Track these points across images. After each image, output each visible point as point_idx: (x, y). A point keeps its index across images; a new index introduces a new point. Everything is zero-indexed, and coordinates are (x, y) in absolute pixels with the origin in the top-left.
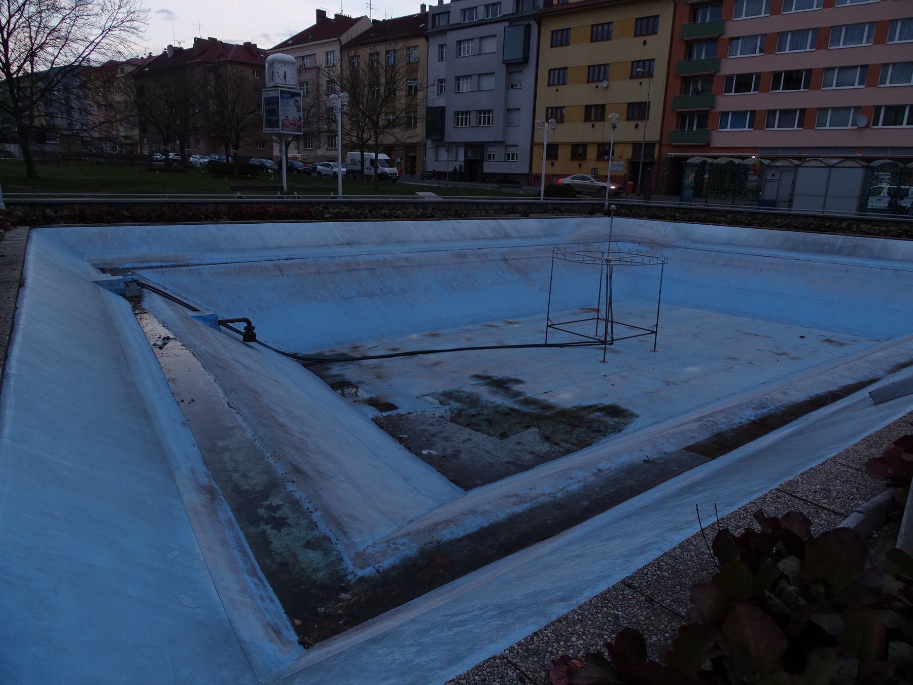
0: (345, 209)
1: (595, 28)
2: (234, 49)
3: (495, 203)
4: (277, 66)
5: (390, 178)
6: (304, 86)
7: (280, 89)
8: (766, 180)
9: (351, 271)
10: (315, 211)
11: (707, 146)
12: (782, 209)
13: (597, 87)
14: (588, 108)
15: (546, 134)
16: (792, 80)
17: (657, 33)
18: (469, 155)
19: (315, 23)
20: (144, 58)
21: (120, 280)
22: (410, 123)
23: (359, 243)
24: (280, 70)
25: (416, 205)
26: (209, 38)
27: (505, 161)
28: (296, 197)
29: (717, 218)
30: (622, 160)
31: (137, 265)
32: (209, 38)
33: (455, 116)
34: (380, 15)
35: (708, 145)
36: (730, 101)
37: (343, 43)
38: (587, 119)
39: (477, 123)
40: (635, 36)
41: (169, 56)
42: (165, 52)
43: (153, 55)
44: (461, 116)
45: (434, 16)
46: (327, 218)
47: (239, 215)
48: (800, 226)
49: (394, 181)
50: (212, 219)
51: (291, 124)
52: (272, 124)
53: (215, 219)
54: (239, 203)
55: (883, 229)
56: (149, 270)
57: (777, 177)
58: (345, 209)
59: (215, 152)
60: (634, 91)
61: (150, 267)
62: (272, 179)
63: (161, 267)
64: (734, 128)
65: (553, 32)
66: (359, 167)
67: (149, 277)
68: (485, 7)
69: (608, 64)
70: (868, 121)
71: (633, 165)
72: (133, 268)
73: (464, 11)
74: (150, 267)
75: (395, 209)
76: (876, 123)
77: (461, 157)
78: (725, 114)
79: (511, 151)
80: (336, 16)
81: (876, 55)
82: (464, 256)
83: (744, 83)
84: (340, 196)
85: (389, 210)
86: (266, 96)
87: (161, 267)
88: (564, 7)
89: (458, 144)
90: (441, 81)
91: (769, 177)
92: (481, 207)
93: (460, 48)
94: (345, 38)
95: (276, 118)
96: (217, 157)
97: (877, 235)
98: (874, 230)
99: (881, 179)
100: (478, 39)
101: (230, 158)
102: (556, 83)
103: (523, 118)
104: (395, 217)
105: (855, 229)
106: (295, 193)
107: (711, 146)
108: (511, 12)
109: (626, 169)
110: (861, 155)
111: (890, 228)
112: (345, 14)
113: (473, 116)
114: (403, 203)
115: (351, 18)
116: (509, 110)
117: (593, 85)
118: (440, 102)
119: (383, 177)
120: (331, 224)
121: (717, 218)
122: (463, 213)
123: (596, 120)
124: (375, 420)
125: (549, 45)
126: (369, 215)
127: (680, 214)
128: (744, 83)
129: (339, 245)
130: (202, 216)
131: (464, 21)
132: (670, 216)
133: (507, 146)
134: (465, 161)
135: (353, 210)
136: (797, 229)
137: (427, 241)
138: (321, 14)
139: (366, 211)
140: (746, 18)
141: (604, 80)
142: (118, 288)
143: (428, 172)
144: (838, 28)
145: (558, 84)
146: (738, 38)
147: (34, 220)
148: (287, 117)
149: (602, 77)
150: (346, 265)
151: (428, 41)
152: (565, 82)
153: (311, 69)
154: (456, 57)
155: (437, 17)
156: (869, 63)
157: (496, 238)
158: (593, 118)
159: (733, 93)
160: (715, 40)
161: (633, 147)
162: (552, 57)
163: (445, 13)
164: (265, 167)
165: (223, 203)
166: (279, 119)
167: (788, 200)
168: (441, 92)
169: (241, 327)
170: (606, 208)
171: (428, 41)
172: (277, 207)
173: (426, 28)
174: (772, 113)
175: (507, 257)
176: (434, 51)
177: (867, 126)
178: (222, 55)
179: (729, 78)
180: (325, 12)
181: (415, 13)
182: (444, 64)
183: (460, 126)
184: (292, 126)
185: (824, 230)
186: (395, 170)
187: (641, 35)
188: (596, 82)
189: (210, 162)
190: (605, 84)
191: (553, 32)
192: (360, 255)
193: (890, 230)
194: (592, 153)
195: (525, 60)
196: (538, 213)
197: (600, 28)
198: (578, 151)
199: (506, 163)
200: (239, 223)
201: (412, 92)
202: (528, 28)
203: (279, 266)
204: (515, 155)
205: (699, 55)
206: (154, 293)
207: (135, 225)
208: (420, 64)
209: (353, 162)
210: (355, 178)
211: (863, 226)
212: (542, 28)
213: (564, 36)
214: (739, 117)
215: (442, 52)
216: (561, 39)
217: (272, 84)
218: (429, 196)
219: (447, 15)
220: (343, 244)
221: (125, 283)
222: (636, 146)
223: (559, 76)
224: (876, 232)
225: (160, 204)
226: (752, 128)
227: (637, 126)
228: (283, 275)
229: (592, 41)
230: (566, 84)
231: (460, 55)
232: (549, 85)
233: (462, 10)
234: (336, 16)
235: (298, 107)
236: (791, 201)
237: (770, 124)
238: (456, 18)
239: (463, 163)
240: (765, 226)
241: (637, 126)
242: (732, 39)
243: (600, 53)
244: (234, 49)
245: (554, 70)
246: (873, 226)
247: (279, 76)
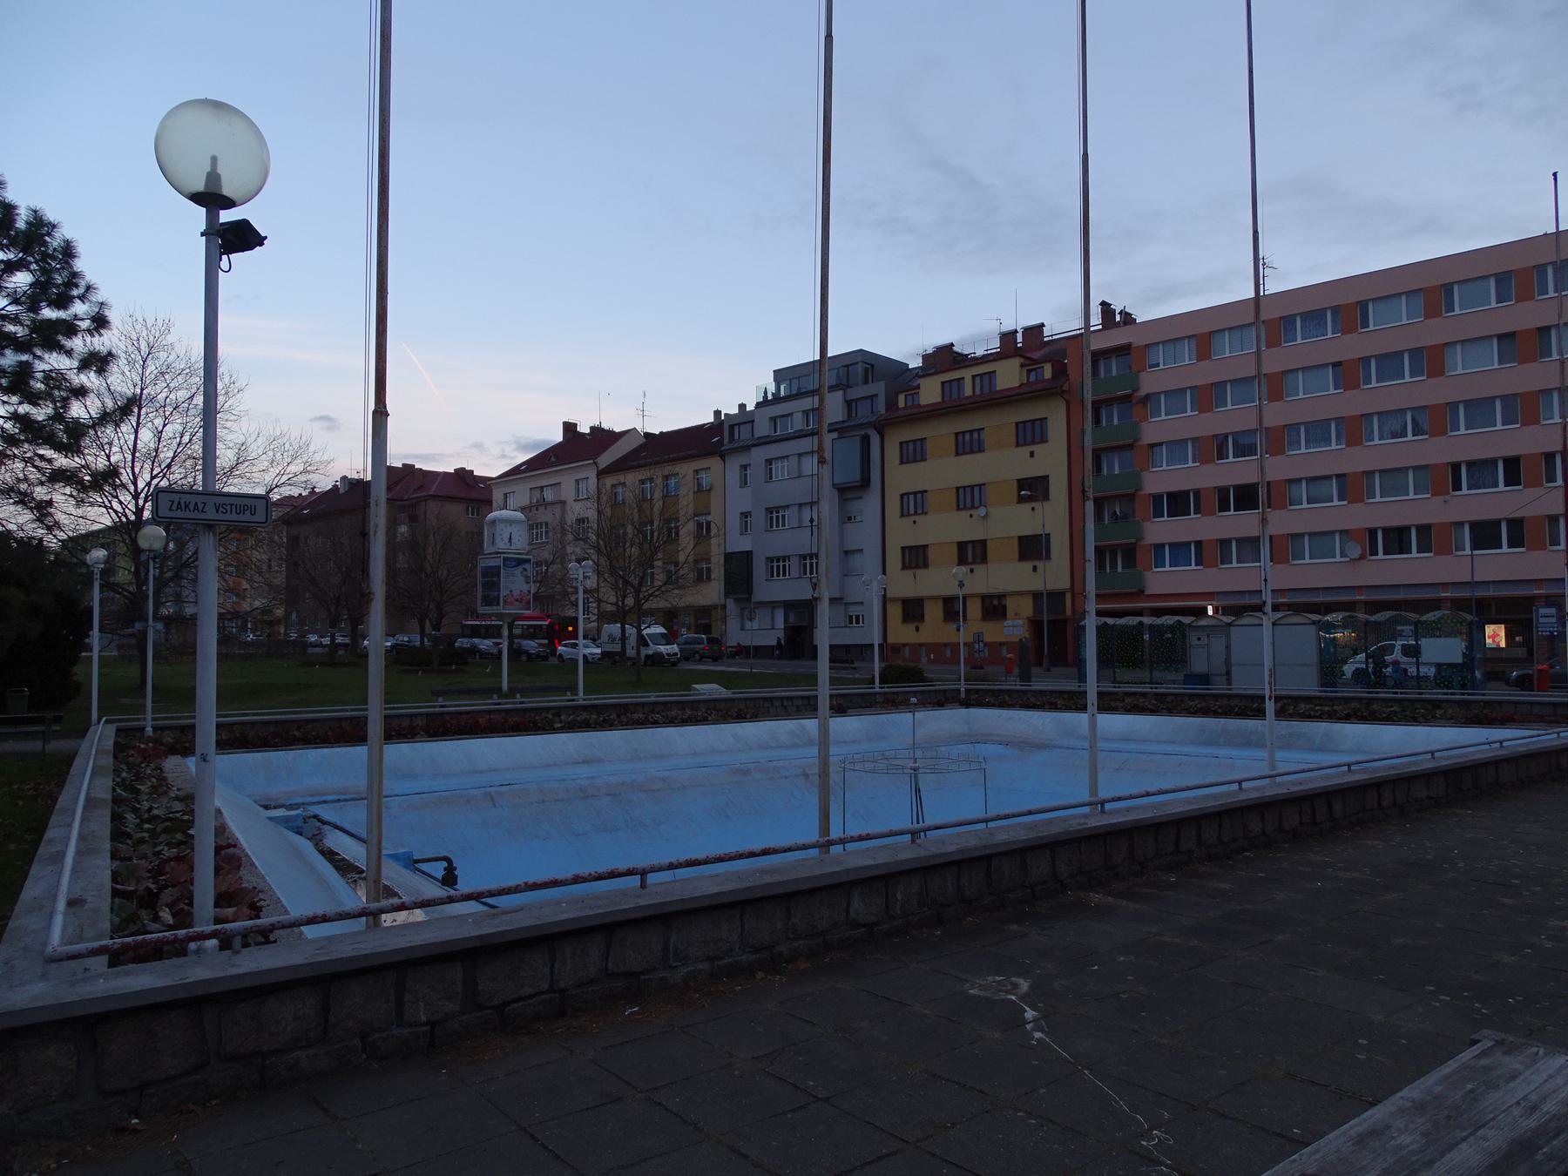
0: (584, 716)
1: (960, 436)
2: (439, 478)
3: (797, 697)
4: (499, 527)
5: (668, 660)
6: (542, 528)
7: (502, 555)
8: (1190, 646)
9: (587, 797)
10: (542, 720)
11: (1140, 593)
12: (1219, 688)
13: (971, 516)
14: (962, 546)
15: (906, 585)
16: (1246, 497)
17: (1047, 441)
18: (792, 619)
19: (561, 439)
20: (304, 494)
21: (298, 816)
22: (703, 577)
23: (600, 761)
24: (503, 532)
25: (694, 705)
26: (403, 464)
27: (846, 627)
28: (518, 702)
29: (1112, 704)
30: (1019, 619)
31: (308, 799)
32: (403, 464)
33: (767, 565)
34: (657, 425)
35: (1142, 592)
36: (1162, 529)
37: (601, 466)
38: (962, 561)
39: (800, 572)
40: (1018, 445)
41: (342, 491)
42: (335, 487)
43: (317, 490)
44: (777, 564)
45: (732, 427)
46: (558, 729)
47: (441, 730)
48: (1220, 711)
49: (674, 664)
50: (405, 736)
51: (517, 600)
52: (490, 601)
53: (409, 736)
54: (441, 714)
55: (1326, 709)
56: (324, 805)
57: (1204, 641)
58: (584, 716)
59: (402, 630)
60: (1016, 520)
61: (325, 802)
62: (488, 670)
63: (339, 800)
64: (1175, 566)
65: (901, 443)
66: (617, 648)
67: (324, 812)
69: (984, 484)
70: (1362, 548)
71: (1035, 624)
72: (303, 804)
73: (774, 420)
74: (325, 802)
75: (652, 712)
76: (1374, 552)
77: (780, 623)
78: (1159, 548)
79: (854, 610)
80: (592, 428)
81: (1356, 461)
82: (746, 772)
83: (1178, 503)
84: (581, 697)
85: (644, 713)
86: (483, 565)
87: (339, 800)
88: (914, 411)
89: (773, 605)
90: (745, 515)
91: (1194, 642)
92: (777, 703)
93: (771, 469)
94: (605, 459)
95: (496, 594)
96: (406, 639)
97: (1320, 717)
98: (1317, 711)
99: (1399, 631)
101: (426, 640)
102: (912, 512)
103: (868, 561)
104: (652, 723)
105: (1291, 711)
106: (518, 696)
107: (1146, 593)
108: (840, 419)
109: (1027, 631)
110: (1363, 597)
111: (1335, 707)
112: (605, 426)
113: (794, 563)
114: (665, 704)
115: (613, 432)
116: (846, 552)
117: (965, 514)
118: (741, 544)
119: (656, 660)
120: (563, 736)
121: (1112, 704)
122: (748, 713)
123: (974, 563)
125: (898, 461)
126: (616, 722)
127: (1064, 699)
128: (1178, 503)
129: (572, 764)
130: (393, 733)
131: (775, 432)
132: (1051, 704)
133: (847, 604)
134: (785, 628)
135: (594, 716)
136: (1216, 714)
137: (695, 754)
138: (569, 428)
139: (612, 717)
140: (1167, 418)
141: (981, 505)
142: (294, 824)
143: (732, 647)
144: (1294, 427)
145: (916, 513)
146: (1160, 444)
147: (185, 747)
148: (511, 591)
149: (977, 504)
150: (581, 790)
151: (724, 461)
152: (925, 511)
153: (552, 503)
154: (766, 482)
155: (736, 428)
156: (1346, 472)
157: (795, 745)
158: (970, 560)
159: (1166, 518)
160: (1130, 447)
161: (1034, 599)
162: (902, 478)
163: (749, 422)
164: (478, 651)
165: (421, 715)
166: (499, 595)
167: (1225, 672)
168: (746, 531)
169: (438, 869)
170: (963, 695)
171: (724, 461)
172: (492, 716)
173: (721, 442)
174: (1225, 543)
175: (808, 772)
176: (733, 475)
177: (1362, 557)
178: (420, 488)
179: (1157, 498)
180: (576, 424)
181: (706, 422)
182: (747, 491)
183: (775, 578)
184: (517, 603)
185: (1251, 714)
186: (674, 648)
187: (1026, 444)
188: (969, 509)
189: (393, 647)
190: (982, 511)
191: (901, 443)
192: (600, 776)
193: (1335, 711)
194: (975, 610)
195: (865, 483)
196: (861, 707)
197: (967, 437)
198: (951, 608)
199: (848, 629)
200: (441, 740)
201: (703, 532)
202: (866, 440)
203: (490, 795)
204: (861, 617)
205: (1111, 468)
206: (337, 831)
207: (308, 748)
208: (713, 493)
209: (612, 639)
210: (614, 663)
211: (1302, 707)
212: (886, 437)
213: (918, 449)
214: (1179, 551)
215: (746, 475)
216: (914, 453)
217: (492, 550)
218: (709, 690)
219: (750, 424)
220: (578, 763)
221: (304, 819)
222: (1036, 596)
223: (915, 503)
224: (1318, 714)
225: (340, 719)
226: (1202, 565)
227: (1035, 569)
228: (495, 806)
229: (957, 454)
230: (926, 513)
231: (771, 479)
232: (902, 515)
233: (771, 418)
234: (592, 428)
235: (527, 577)
236: (1228, 673)
237: (1226, 559)
238: (763, 429)
239: (783, 631)
240: (1175, 711)
241: (1035, 569)
242: (1152, 446)
243: (970, 469)
244: (439, 478)
245: (908, 494)
246: (1316, 705)
247: (502, 539)
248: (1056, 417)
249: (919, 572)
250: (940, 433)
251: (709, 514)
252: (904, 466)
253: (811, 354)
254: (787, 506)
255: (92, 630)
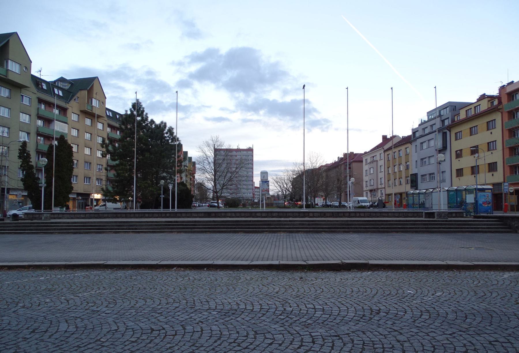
68: (430, 127)
100: (427, 141)
113: (428, 176)
124: (112, 187)
162: (456, 145)
212: (451, 133)
233: (423, 129)
248: (498, 117)
249: (461, 178)
250: (465, 128)
251: (408, 162)
252: (456, 141)
253: (435, 108)
254: (425, 158)
255: (305, 204)
